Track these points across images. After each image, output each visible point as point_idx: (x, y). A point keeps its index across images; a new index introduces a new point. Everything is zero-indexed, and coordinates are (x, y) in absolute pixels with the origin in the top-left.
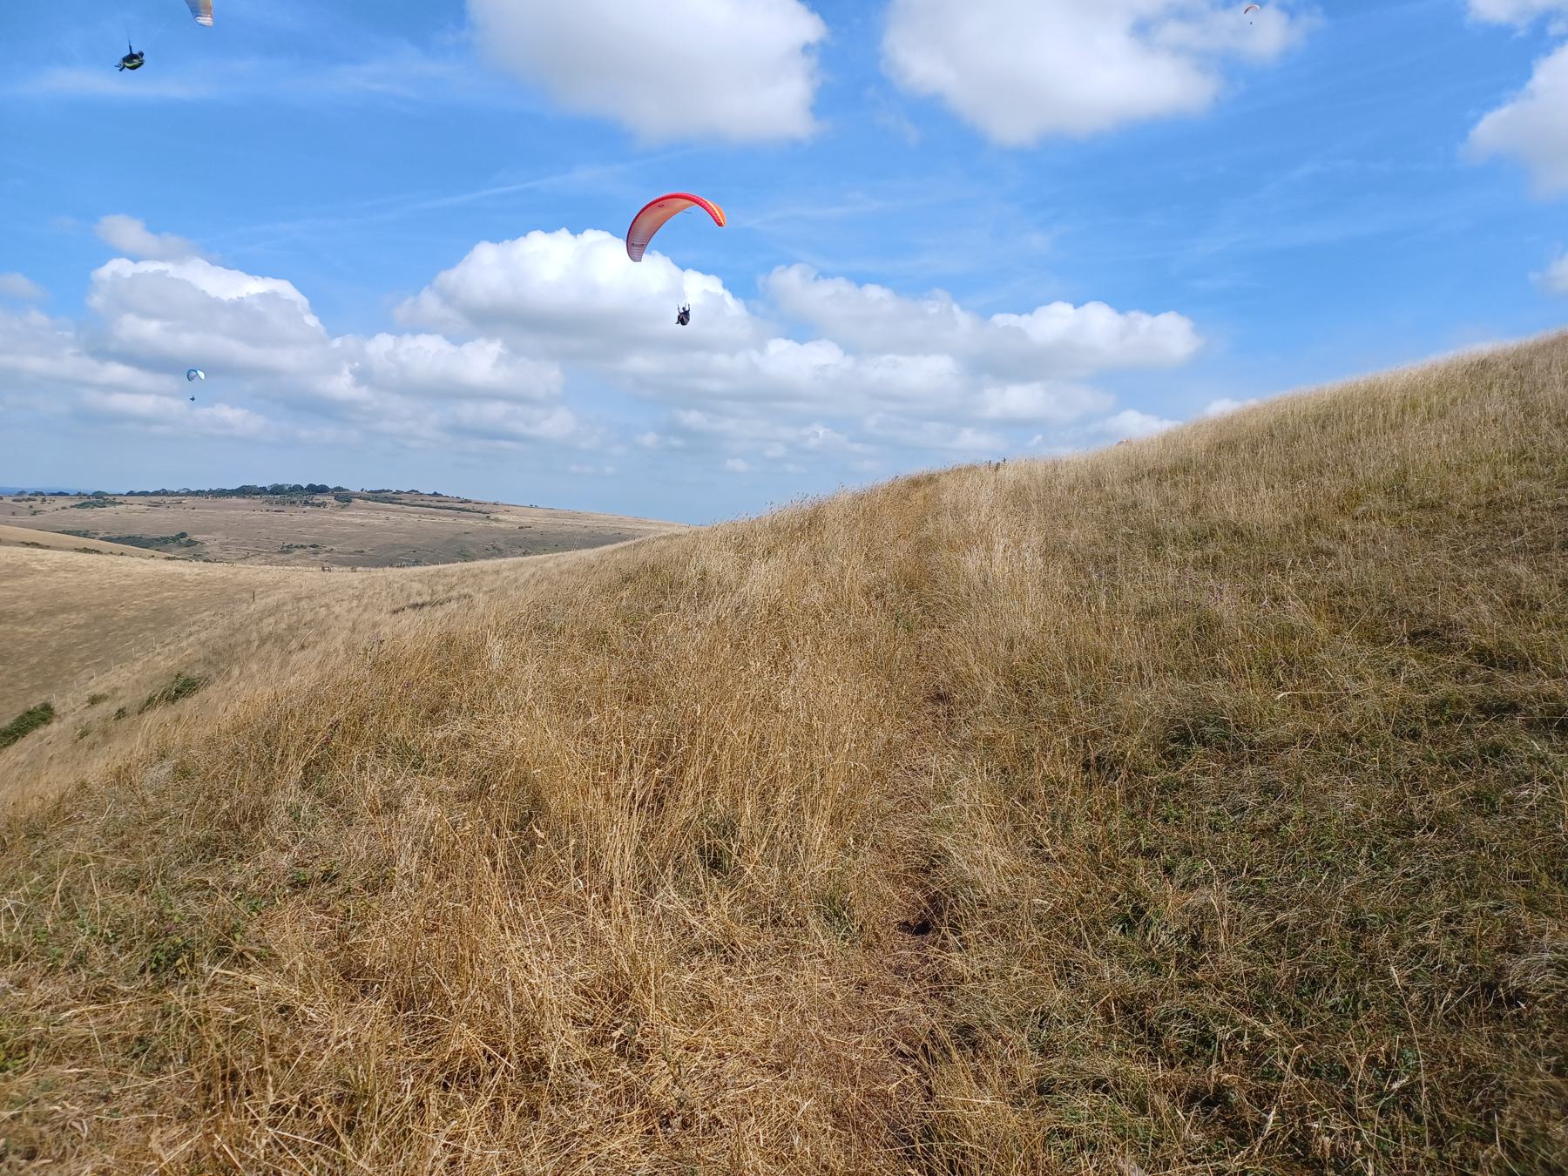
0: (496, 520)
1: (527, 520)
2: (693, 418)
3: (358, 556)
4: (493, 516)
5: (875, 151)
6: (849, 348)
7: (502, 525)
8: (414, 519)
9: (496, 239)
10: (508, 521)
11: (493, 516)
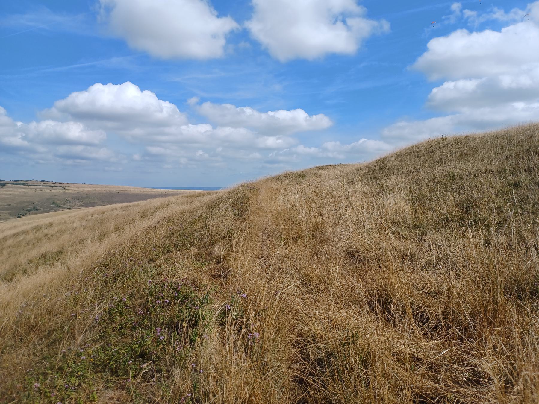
0: (68, 190)
1: (80, 189)
2: (154, 150)
3: (9, 207)
4: (66, 188)
5: (251, 66)
6: (215, 125)
7: (71, 192)
8: (34, 191)
9: (315, 115)
10: (73, 190)
11: (66, 188)
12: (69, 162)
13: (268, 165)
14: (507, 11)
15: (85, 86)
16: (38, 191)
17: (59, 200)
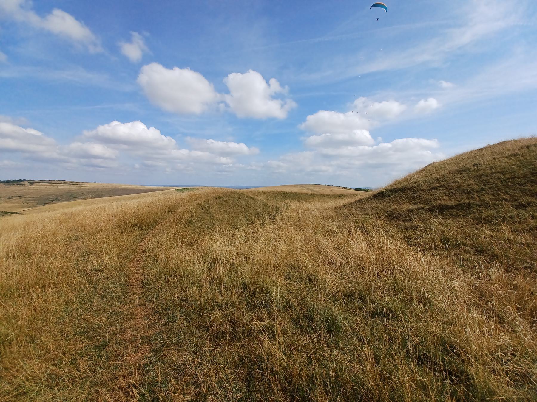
2: (149, 162)
10: (87, 186)
12: (91, 169)
13: (219, 173)
14: (426, 101)
15: (108, 121)
16: (60, 187)
17: (75, 193)
